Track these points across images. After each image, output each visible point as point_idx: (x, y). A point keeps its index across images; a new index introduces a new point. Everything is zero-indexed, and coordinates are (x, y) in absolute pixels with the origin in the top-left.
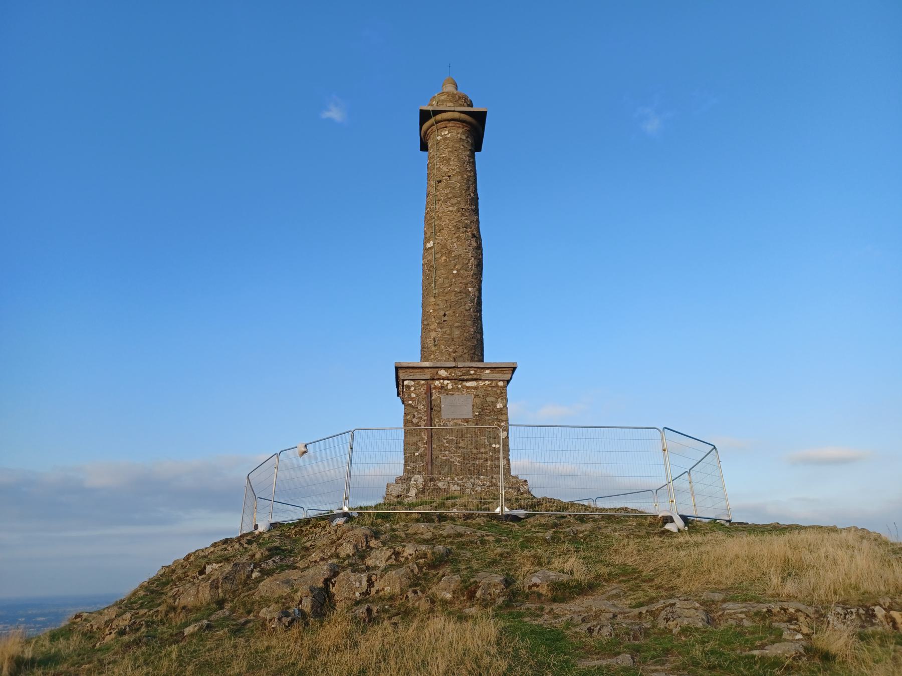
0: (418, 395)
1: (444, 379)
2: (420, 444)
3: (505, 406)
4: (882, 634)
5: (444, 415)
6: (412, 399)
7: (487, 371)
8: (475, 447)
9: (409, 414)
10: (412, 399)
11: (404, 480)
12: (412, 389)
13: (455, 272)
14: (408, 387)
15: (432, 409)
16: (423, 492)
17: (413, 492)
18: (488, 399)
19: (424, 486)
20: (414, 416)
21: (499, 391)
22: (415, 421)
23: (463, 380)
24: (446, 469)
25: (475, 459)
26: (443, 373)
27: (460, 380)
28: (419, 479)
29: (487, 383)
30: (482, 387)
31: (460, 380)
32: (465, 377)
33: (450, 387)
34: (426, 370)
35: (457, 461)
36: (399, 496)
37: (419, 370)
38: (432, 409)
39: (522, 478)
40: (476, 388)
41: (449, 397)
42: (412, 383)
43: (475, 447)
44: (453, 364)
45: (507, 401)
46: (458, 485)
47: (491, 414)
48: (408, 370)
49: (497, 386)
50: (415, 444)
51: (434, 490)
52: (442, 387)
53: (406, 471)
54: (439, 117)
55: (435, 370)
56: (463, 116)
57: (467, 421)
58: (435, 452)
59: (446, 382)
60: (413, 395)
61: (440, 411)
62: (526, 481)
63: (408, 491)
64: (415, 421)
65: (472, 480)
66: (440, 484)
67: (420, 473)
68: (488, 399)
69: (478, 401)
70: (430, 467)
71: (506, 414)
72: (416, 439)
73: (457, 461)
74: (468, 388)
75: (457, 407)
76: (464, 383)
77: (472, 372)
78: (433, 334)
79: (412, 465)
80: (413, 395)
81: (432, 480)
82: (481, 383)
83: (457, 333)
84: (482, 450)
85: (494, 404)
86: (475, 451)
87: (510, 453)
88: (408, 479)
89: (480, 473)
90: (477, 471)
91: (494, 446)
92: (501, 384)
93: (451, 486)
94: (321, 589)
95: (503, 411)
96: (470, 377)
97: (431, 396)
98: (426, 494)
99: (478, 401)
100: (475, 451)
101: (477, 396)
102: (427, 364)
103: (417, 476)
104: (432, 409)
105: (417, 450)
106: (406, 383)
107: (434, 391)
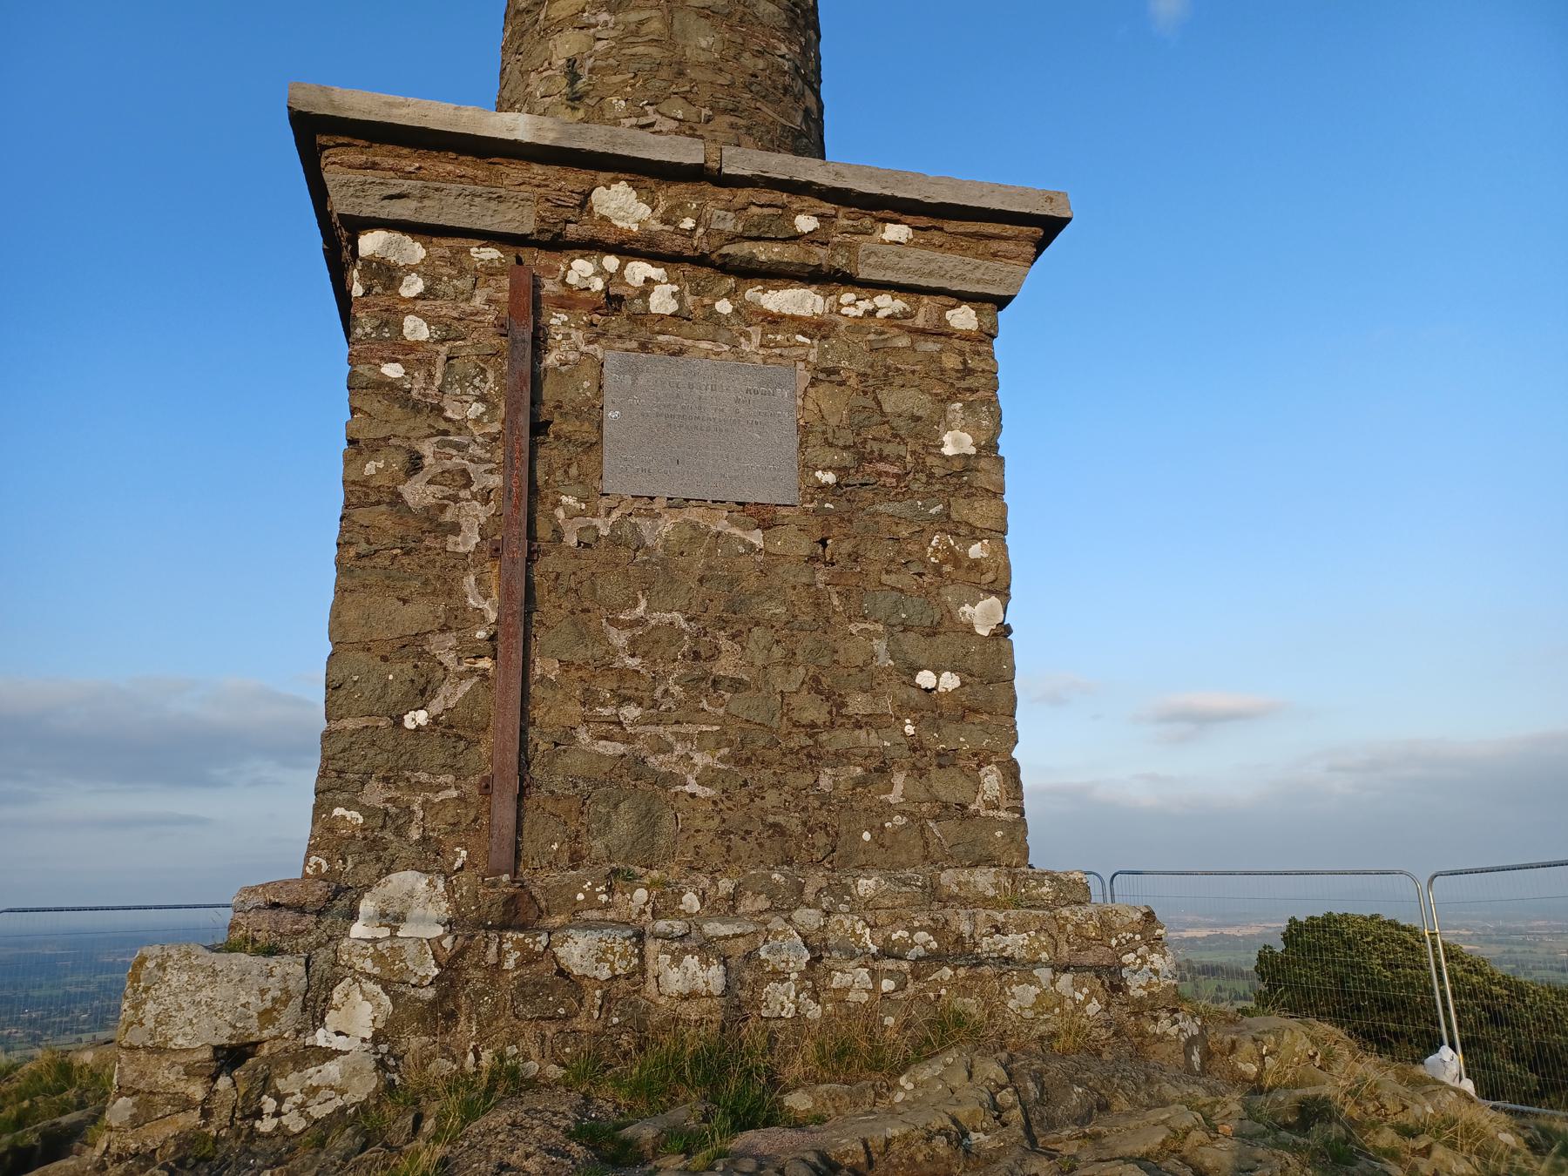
0: (447, 332)
1: (627, 249)
2: (444, 649)
3: (989, 448)
4: (960, 939)
5: (622, 473)
6: (403, 350)
7: (896, 232)
8: (815, 684)
9: (375, 447)
11: (299, 920)
12: (413, 286)
14: (385, 273)
15: (539, 428)
16: (439, 1014)
17: (357, 1015)
18: (893, 401)
19: (451, 967)
20: (415, 464)
21: (951, 362)
22: (417, 493)
24: (624, 824)
25: (813, 759)
26: (621, 205)
27: (726, 267)
28: (414, 910)
29: (887, 304)
30: (857, 325)
31: (726, 267)
32: (764, 253)
33: (662, 301)
34: (514, 172)
35: (695, 767)
36: (232, 1056)
37: (467, 166)
38: (539, 428)
39: (1130, 899)
40: (818, 328)
41: (656, 368)
42: (415, 251)
43: (815, 684)
44: (689, 153)
45: (997, 416)
46: (707, 948)
47: (908, 513)
48: (384, 155)
49: (942, 332)
50: (413, 645)
51: (528, 991)
52: (613, 302)
53: (326, 837)
55: (574, 179)
57: (765, 517)
58: (552, 712)
59: (639, 271)
61: (593, 447)
62: (1149, 916)
63: (315, 1009)
64: (417, 493)
65: (808, 917)
66: (577, 951)
67: (430, 856)
68: (893, 401)
69: (833, 405)
70: (505, 812)
71: (997, 493)
72: (415, 615)
73: (695, 767)
74: (775, 320)
75: (704, 427)
76: (751, 293)
77: (805, 223)
78: (565, 45)
79: (375, 794)
80: (416, 329)
81: (517, 913)
82: (852, 305)
83: (703, 41)
84: (858, 704)
85: (925, 431)
86: (814, 711)
88: (335, 900)
89: (840, 859)
90: (816, 846)
91: (925, 679)
92: (963, 318)
93: (658, 961)
95: (978, 478)
97: (539, 342)
98: (466, 1029)
99: (833, 405)
100: (814, 711)
101: (826, 374)
102: (518, 126)
103: (407, 882)
104: (540, 425)
105: (422, 694)
106: (370, 243)
107: (557, 319)
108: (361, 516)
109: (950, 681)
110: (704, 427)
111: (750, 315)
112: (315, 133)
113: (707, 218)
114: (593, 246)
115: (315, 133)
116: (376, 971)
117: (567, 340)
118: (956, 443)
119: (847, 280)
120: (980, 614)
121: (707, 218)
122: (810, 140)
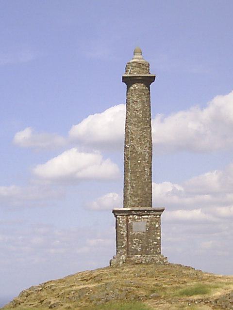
3: (159, 226)
5: (134, 229)
12: (121, 219)
14: (119, 218)
33: (136, 218)
35: (139, 249)
42: (121, 217)
49: (157, 217)
68: (152, 223)
73: (139, 249)
74: (144, 218)
82: (150, 216)
92: (158, 216)
106: (118, 216)
108: (149, 191)
110: (140, 225)
111: (142, 218)
112: (114, 212)
115: (114, 212)
117: (130, 221)
118: (157, 226)
120: (159, 238)
122: (151, 206)
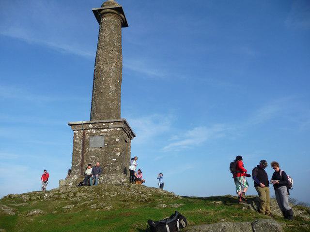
1: (92, 129)
5: (91, 145)
6: (77, 139)
7: (112, 124)
10: (77, 139)
12: (77, 134)
13: (104, 79)
23: (101, 129)
26: (91, 126)
29: (112, 129)
30: (109, 132)
32: (101, 127)
33: (94, 132)
40: (106, 132)
42: (77, 132)
49: (117, 131)
54: (103, 11)
56: (112, 10)
60: (77, 137)
82: (109, 130)
84: (108, 162)
85: (115, 139)
87: (121, 111)
91: (115, 160)
94: (118, 116)
96: (103, 127)
109: (115, 160)
113: (97, 125)
114: (89, 129)
116: (105, 208)
119: (109, 128)
121: (97, 125)
122: (120, 118)
